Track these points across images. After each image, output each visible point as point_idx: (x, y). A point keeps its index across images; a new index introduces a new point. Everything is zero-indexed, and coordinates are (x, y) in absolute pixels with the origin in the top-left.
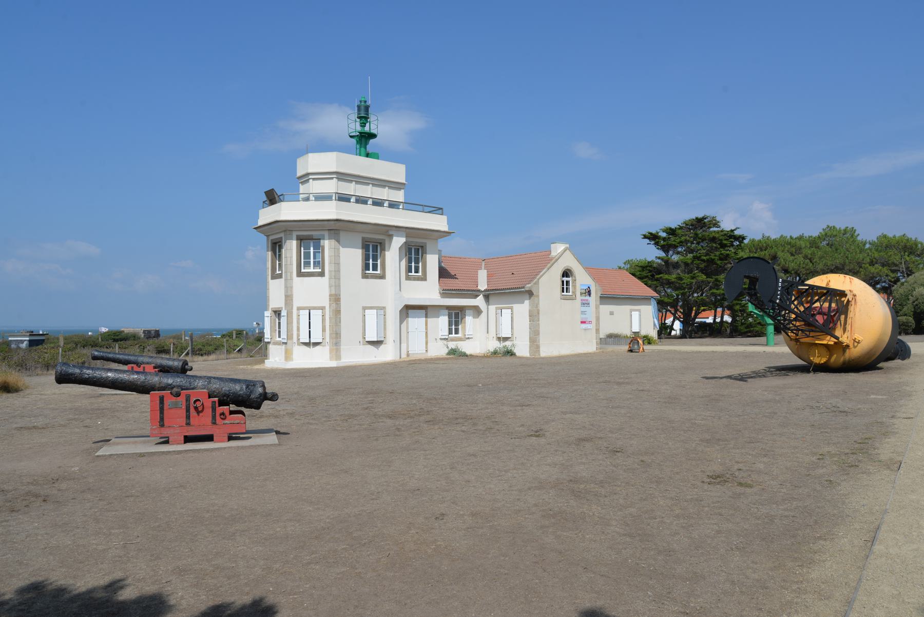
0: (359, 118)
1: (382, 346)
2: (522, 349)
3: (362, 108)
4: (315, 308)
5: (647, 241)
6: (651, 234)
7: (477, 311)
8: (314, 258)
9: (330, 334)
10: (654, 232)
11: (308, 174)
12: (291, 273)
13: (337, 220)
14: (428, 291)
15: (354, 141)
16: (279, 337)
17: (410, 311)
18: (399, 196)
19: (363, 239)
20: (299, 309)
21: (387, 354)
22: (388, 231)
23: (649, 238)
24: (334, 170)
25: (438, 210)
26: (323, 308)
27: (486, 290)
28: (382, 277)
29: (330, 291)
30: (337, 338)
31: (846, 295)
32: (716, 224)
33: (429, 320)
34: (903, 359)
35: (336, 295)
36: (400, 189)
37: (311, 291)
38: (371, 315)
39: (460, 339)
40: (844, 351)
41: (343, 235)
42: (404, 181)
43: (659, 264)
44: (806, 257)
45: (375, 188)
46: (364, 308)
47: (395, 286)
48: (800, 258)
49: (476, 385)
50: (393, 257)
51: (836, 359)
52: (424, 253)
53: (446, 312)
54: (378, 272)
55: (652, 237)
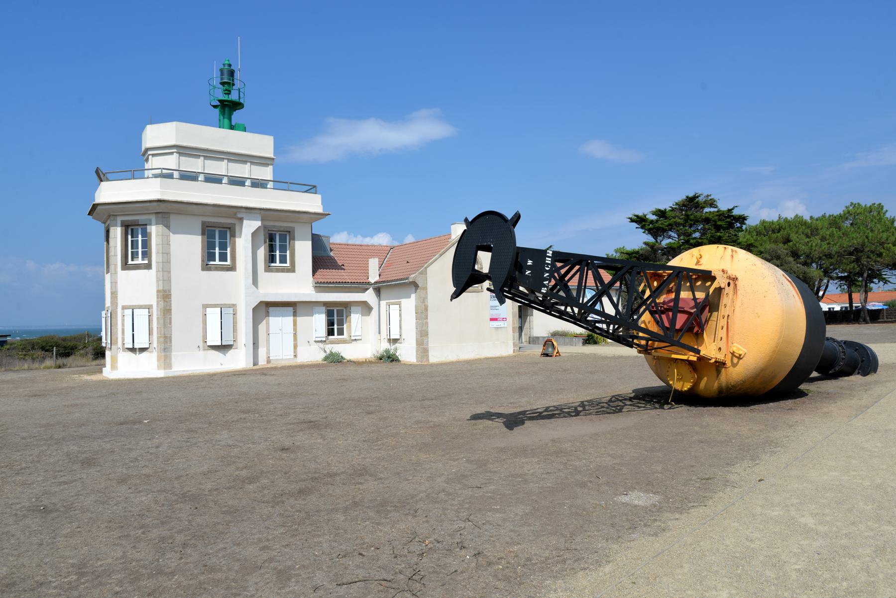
0: (223, 84)
1: (231, 352)
2: (407, 353)
3: (225, 72)
4: (140, 307)
5: (635, 225)
7: (366, 308)
8: (132, 248)
9: (158, 338)
10: (640, 214)
12: (116, 265)
13: (159, 201)
14: (298, 283)
15: (217, 110)
16: (504, 319)
17: (271, 309)
19: (203, 223)
20: (124, 308)
21: (238, 360)
22: (237, 213)
23: (636, 222)
24: (173, 143)
25: (312, 189)
26: (149, 307)
27: (376, 283)
28: (232, 268)
29: (158, 285)
30: (165, 342)
31: (713, 279)
32: (712, 204)
33: (299, 319)
34: (865, 374)
35: (164, 291)
36: (267, 165)
37: (132, 288)
38: (213, 315)
39: (344, 342)
40: (718, 372)
41: (173, 219)
42: (272, 156)
43: (647, 251)
44: (823, 239)
46: (205, 306)
47: (245, 279)
48: (816, 241)
49: (140, 422)
50: (243, 244)
51: (708, 384)
52: (293, 238)
53: (324, 309)
54: (228, 263)
55: (640, 221)
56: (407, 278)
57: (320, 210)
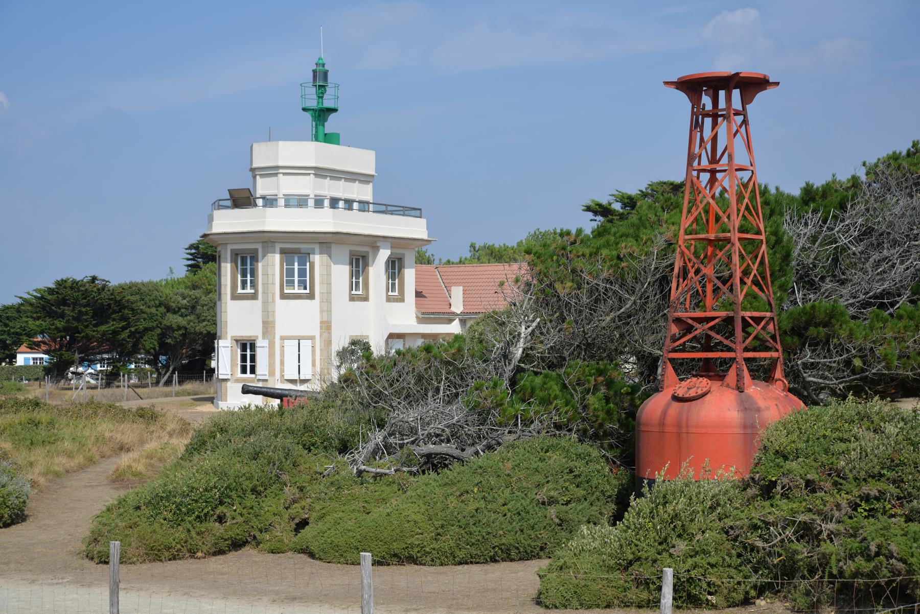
5: (590, 215)
6: (600, 205)
10: (604, 202)
11: (278, 167)
12: (274, 294)
18: (365, 192)
20: (283, 338)
22: (374, 242)
26: (312, 338)
29: (322, 316)
36: (367, 182)
41: (334, 249)
42: (373, 173)
45: (333, 182)
50: (377, 271)
56: (194, 399)
57: (425, 237)
